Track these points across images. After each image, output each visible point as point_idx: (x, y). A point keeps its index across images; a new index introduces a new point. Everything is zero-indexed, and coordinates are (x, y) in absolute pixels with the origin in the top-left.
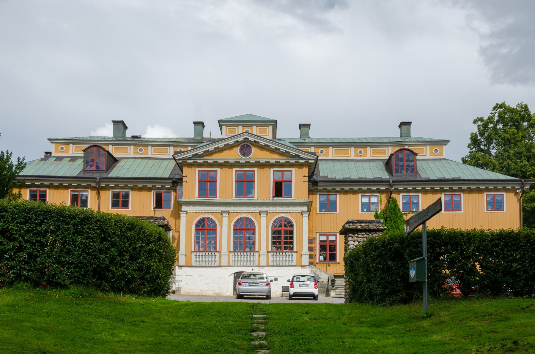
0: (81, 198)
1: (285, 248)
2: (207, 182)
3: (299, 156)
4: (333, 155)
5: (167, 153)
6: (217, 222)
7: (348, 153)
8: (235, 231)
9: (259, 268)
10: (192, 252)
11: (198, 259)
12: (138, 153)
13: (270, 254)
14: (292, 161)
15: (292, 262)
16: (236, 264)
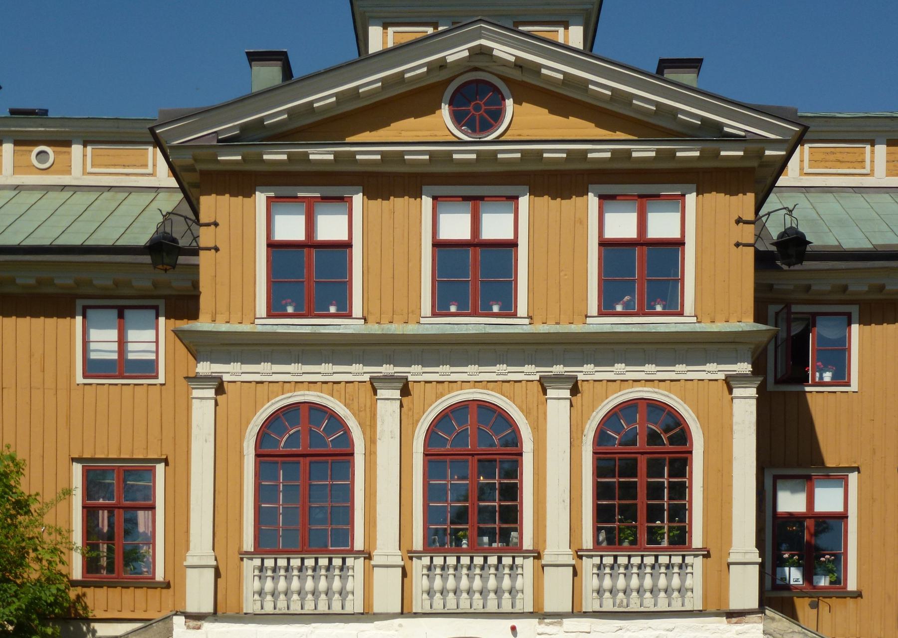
0: (245, 557)
1: (654, 537)
2: (305, 250)
3: (719, 126)
4: (802, 169)
5: (146, 166)
6: (352, 424)
7: (863, 161)
8: (429, 461)
9: (540, 623)
10: (244, 555)
11: (269, 585)
12: (30, 169)
13: (588, 565)
14: (689, 153)
15: (683, 597)
16: (438, 606)
